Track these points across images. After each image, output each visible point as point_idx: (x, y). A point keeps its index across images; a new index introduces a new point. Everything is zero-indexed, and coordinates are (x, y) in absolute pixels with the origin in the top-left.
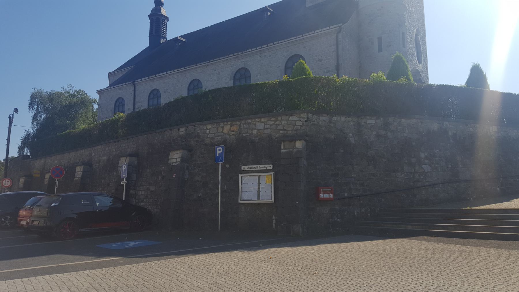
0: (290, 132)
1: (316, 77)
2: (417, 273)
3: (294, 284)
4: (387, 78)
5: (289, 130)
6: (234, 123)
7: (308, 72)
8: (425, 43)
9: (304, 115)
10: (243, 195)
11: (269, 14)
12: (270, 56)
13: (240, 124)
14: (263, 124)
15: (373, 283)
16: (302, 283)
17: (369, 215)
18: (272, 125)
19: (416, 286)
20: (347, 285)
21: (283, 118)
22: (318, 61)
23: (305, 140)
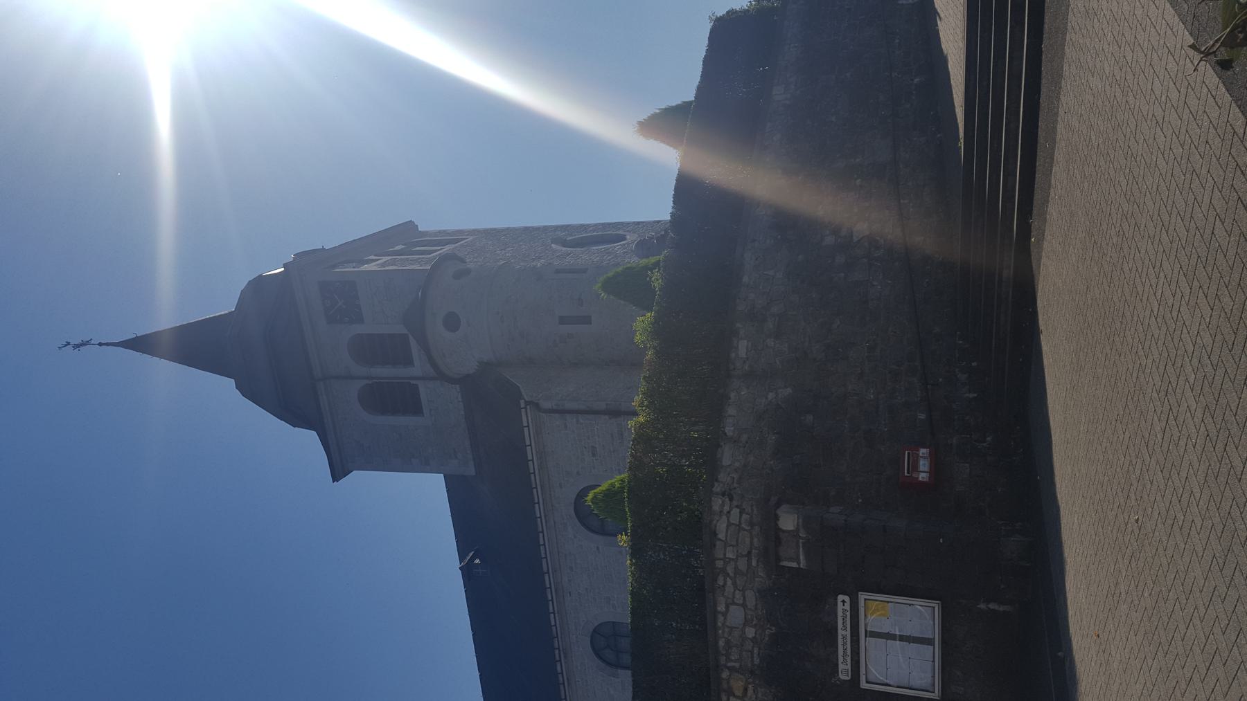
0: (755, 540)
1: (630, 469)
2: (1126, 269)
3: (1169, 584)
4: (650, 310)
5: (751, 543)
6: (725, 686)
7: (617, 485)
8: (582, 225)
9: (717, 503)
10: (917, 682)
11: (477, 561)
12: (571, 568)
13: (728, 668)
14: (732, 608)
15: (1157, 378)
16: (1165, 563)
17: (974, 364)
18: (734, 584)
19: (1162, 275)
20: (1165, 445)
21: (719, 553)
22: (594, 455)
23: (778, 505)
